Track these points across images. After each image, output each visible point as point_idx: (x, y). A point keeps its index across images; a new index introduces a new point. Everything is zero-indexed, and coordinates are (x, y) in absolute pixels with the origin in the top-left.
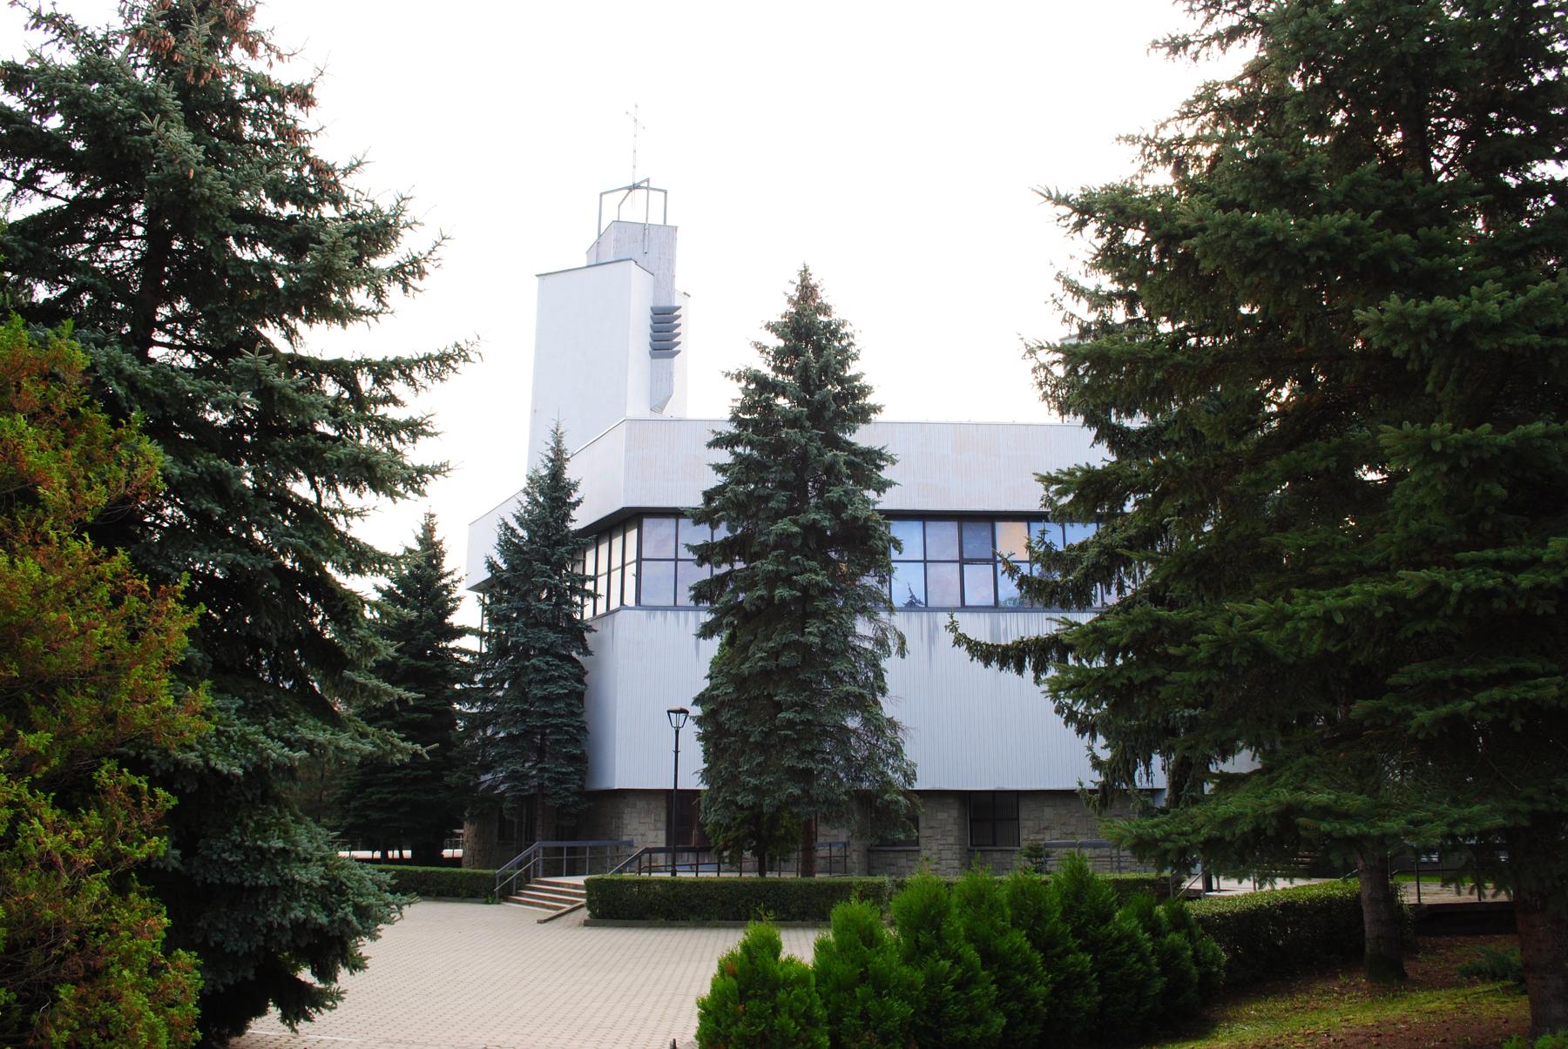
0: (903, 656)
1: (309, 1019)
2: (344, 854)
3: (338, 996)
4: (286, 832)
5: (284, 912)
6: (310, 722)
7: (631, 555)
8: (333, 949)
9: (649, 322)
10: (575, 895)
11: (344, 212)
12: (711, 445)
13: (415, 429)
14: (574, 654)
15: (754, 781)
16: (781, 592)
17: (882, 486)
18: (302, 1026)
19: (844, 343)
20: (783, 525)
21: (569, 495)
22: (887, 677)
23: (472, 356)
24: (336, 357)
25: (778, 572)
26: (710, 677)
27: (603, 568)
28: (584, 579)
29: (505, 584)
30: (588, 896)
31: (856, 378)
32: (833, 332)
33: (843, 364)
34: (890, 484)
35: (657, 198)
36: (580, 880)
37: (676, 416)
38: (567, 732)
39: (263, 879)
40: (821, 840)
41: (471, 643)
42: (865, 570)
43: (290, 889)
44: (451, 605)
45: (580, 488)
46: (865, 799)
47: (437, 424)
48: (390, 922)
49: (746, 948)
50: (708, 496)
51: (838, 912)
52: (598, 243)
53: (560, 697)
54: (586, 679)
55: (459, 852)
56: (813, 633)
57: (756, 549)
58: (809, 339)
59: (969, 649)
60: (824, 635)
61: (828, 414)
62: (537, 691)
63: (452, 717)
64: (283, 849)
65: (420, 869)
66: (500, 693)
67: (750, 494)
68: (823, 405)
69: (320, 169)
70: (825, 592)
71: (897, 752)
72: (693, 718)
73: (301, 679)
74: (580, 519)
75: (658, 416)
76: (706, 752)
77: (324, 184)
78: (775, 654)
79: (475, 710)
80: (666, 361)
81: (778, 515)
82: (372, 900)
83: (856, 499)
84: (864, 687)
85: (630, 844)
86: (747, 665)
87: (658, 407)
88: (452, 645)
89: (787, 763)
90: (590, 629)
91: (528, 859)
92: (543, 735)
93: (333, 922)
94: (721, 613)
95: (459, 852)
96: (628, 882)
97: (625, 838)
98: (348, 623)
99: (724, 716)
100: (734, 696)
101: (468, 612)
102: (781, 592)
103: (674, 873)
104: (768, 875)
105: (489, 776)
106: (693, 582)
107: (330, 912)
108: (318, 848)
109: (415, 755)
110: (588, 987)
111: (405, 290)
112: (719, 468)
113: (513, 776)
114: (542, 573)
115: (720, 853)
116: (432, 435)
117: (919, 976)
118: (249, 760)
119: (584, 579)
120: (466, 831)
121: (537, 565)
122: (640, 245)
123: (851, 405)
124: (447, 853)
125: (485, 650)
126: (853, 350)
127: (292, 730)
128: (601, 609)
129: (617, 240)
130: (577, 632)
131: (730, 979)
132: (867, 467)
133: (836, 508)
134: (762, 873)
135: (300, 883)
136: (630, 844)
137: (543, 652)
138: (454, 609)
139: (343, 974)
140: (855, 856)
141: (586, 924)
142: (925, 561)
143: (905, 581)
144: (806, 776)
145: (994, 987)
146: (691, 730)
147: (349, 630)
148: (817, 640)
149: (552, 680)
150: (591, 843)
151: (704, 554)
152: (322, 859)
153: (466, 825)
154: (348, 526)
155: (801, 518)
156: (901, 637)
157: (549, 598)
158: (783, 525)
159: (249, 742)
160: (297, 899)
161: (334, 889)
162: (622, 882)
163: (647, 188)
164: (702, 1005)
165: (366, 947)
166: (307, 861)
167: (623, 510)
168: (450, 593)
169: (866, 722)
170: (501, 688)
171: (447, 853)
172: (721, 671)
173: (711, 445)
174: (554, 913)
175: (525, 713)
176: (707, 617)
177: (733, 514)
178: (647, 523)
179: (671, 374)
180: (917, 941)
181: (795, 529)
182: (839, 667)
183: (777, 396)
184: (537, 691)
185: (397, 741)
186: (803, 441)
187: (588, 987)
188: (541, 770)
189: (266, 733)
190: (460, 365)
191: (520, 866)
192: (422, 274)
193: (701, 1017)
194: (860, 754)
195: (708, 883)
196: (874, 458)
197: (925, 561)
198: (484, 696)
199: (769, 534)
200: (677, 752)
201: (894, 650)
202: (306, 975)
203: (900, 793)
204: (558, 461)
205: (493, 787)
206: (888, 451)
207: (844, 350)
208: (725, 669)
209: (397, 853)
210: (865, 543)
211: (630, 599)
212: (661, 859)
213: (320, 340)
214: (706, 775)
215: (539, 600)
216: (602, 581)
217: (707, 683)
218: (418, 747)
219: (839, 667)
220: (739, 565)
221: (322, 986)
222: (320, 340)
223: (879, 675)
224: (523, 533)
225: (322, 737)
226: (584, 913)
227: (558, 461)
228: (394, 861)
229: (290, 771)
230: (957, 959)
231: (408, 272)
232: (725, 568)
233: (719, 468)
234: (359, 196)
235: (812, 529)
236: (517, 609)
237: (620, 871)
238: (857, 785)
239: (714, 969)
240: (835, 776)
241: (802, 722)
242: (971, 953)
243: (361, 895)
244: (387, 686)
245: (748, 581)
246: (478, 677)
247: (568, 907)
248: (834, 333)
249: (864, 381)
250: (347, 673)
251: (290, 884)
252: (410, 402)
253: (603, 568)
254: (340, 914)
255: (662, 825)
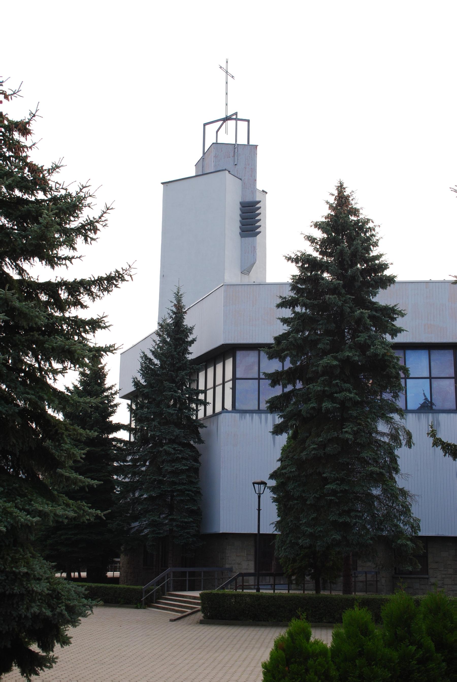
0: (410, 447)
1: (37, 674)
2: (58, 575)
3: (53, 660)
4: (28, 563)
5: (28, 609)
6: (40, 500)
7: (229, 376)
8: (51, 633)
9: (239, 212)
10: (194, 603)
11: (49, 196)
12: (280, 306)
13: (95, 324)
14: (192, 442)
15: (310, 530)
16: (327, 405)
17: (395, 332)
18: (33, 677)
19: (368, 235)
20: (327, 360)
21: (187, 336)
22: (399, 461)
23: (126, 277)
24: (47, 280)
25: (324, 391)
26: (280, 460)
27: (210, 384)
28: (198, 392)
29: (145, 396)
30: (203, 604)
31: (378, 257)
32: (361, 226)
33: (368, 250)
34: (400, 330)
35: (242, 126)
36: (197, 594)
37: (257, 282)
38: (188, 495)
39: (16, 590)
40: (359, 569)
41: (123, 435)
42: (383, 389)
43: (31, 595)
44: (110, 409)
45: (194, 331)
46: (387, 542)
47: (108, 321)
48: (85, 616)
49: (290, 634)
50: (278, 339)
51: (347, 615)
52: (203, 159)
53: (183, 471)
54: (200, 459)
55: (117, 574)
56: (348, 432)
57: (310, 375)
58: (345, 232)
59: (443, 448)
60: (355, 433)
61: (357, 284)
62: (168, 467)
63: (111, 484)
64: (27, 573)
65: (94, 585)
66: (144, 469)
67: (305, 339)
68: (353, 278)
69: (34, 169)
70: (356, 404)
71: (406, 511)
72: (269, 488)
73: (32, 476)
74: (195, 351)
75: (246, 280)
76: (279, 509)
77: (37, 179)
78: (323, 446)
79: (127, 480)
80: (251, 239)
81: (325, 353)
82: (76, 603)
83: (376, 342)
84: (382, 468)
85: (231, 570)
86: (305, 453)
87: (246, 270)
88: (111, 436)
89: (332, 518)
90: (202, 426)
91: (163, 579)
92: (172, 496)
93: (54, 615)
94: (288, 418)
95: (117, 574)
96: (229, 595)
97: (227, 566)
98: (58, 441)
99: (290, 486)
100: (297, 473)
101: (122, 415)
102: (327, 405)
103: (258, 590)
104: (322, 592)
105: (137, 524)
106: (269, 397)
107: (53, 609)
108: (45, 573)
109: (97, 517)
110: (202, 661)
111: (86, 240)
112: (285, 321)
113: (153, 524)
114: (170, 389)
115: (289, 577)
116: (104, 328)
117: (395, 655)
118: (8, 522)
119: (198, 392)
120: (121, 560)
121: (166, 384)
122: (231, 161)
123: (377, 275)
124: (110, 574)
125: (132, 440)
126: (374, 239)
127: (30, 504)
128: (210, 412)
129: (216, 157)
130: (194, 428)
131: (280, 652)
132: (386, 317)
133: (363, 348)
134: (318, 591)
135: (37, 592)
136: (231, 570)
137: (171, 441)
138: (114, 412)
139: (57, 646)
140: (383, 581)
141: (202, 622)
142: (430, 378)
143: (415, 392)
144: (346, 527)
145: (444, 664)
146: (268, 496)
147: (60, 445)
148: (351, 437)
149: (177, 460)
150: (205, 569)
151: (275, 379)
152: (47, 578)
153: (122, 556)
154: (55, 380)
155: (339, 355)
156: (409, 435)
157: (175, 405)
158: (327, 360)
159: (8, 512)
160: (35, 602)
161: (54, 597)
162: (224, 595)
163: (237, 119)
164: (265, 666)
165: (70, 631)
166: (39, 579)
167: (223, 344)
168: (110, 401)
169: (385, 491)
170: (144, 465)
171: (110, 574)
172: (287, 457)
173: (280, 306)
174: (180, 615)
175: (161, 482)
176: (279, 421)
177: (294, 353)
178: (239, 354)
179: (255, 248)
180: (396, 634)
181: (335, 363)
182: (366, 454)
183: (322, 272)
184: (168, 467)
185: (87, 509)
186: (340, 303)
187: (202, 661)
188: (172, 520)
189: (16, 507)
190: (120, 284)
191: (158, 583)
192: (95, 230)
193: (265, 674)
194: (381, 512)
195: (281, 597)
196: (390, 313)
197: (430, 378)
198: (132, 470)
199: (318, 366)
200: (259, 510)
201: (404, 442)
202: (34, 647)
203: (408, 539)
204: (179, 313)
205: (140, 531)
206: (400, 308)
207: (369, 239)
208: (291, 455)
209: (77, 574)
210: (384, 371)
211: (228, 405)
212: (251, 580)
213: (38, 271)
214: (278, 525)
215: (169, 406)
216: (210, 393)
217: (279, 464)
218: (99, 512)
219: (366, 454)
220: (299, 385)
221: (44, 654)
222: (38, 271)
223: (394, 459)
224: (156, 361)
225: (47, 508)
226: (200, 615)
227: (179, 313)
228: (75, 580)
229: (27, 527)
230: (420, 646)
231: (89, 229)
232: (290, 388)
233: (285, 321)
234: (58, 186)
235: (347, 361)
236: (154, 413)
237: (223, 588)
238: (379, 533)
239: (271, 646)
240: (364, 527)
241: (341, 491)
242: (429, 642)
243: (69, 600)
244: (81, 477)
245: (305, 397)
246: (129, 458)
247: (189, 611)
248: (361, 228)
249: (383, 260)
250: (59, 470)
251: (30, 593)
252: (89, 309)
253: (210, 384)
254: (58, 610)
255: (252, 557)
